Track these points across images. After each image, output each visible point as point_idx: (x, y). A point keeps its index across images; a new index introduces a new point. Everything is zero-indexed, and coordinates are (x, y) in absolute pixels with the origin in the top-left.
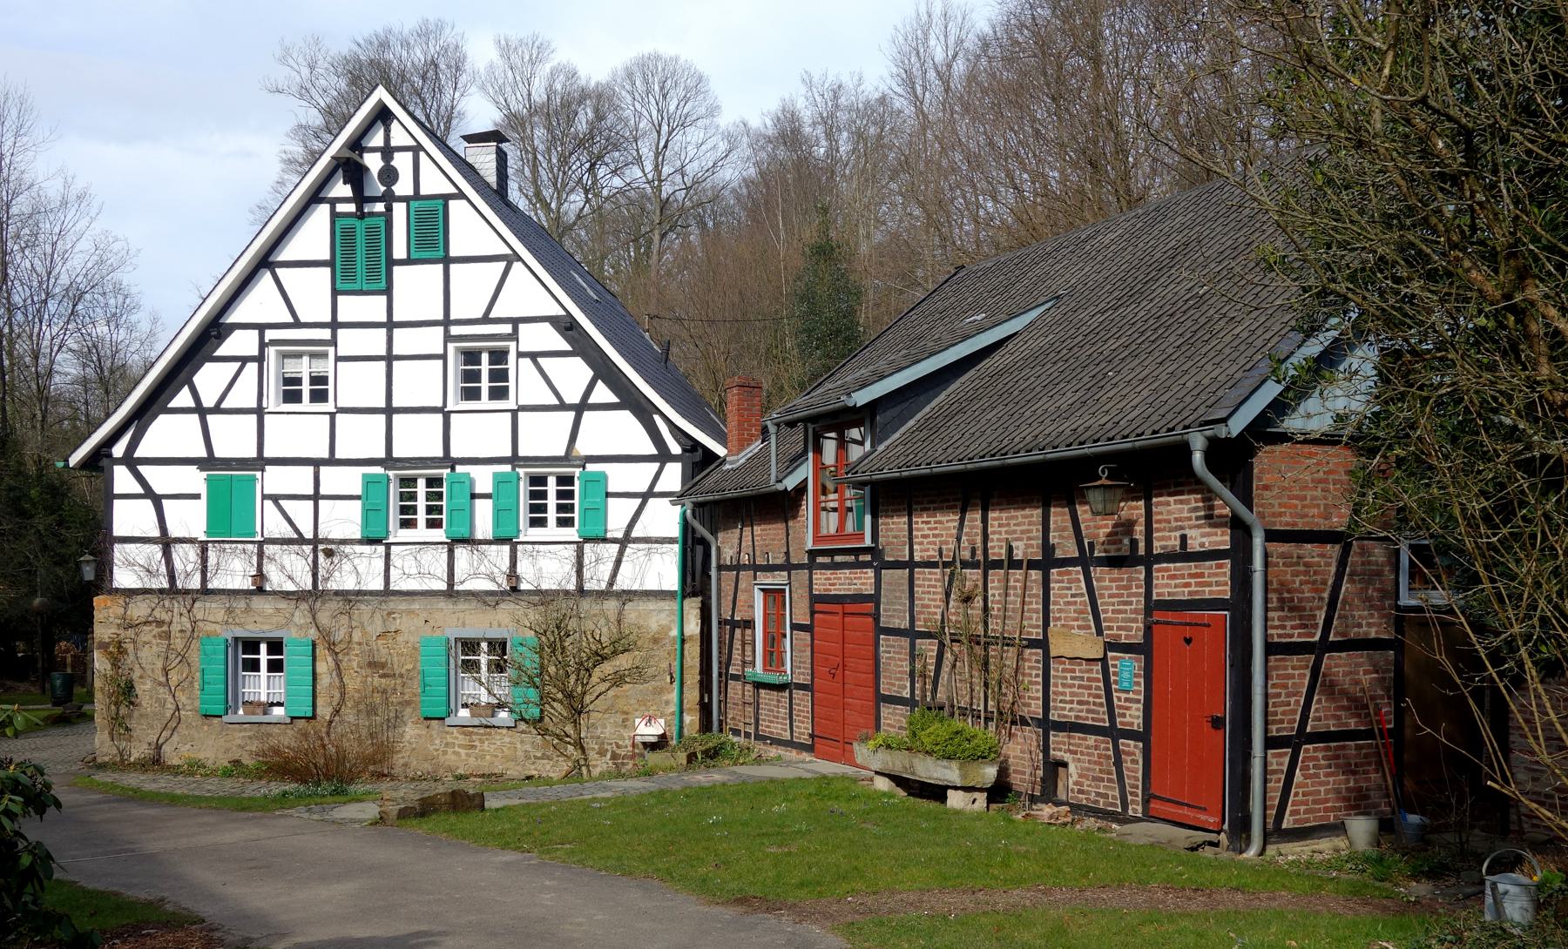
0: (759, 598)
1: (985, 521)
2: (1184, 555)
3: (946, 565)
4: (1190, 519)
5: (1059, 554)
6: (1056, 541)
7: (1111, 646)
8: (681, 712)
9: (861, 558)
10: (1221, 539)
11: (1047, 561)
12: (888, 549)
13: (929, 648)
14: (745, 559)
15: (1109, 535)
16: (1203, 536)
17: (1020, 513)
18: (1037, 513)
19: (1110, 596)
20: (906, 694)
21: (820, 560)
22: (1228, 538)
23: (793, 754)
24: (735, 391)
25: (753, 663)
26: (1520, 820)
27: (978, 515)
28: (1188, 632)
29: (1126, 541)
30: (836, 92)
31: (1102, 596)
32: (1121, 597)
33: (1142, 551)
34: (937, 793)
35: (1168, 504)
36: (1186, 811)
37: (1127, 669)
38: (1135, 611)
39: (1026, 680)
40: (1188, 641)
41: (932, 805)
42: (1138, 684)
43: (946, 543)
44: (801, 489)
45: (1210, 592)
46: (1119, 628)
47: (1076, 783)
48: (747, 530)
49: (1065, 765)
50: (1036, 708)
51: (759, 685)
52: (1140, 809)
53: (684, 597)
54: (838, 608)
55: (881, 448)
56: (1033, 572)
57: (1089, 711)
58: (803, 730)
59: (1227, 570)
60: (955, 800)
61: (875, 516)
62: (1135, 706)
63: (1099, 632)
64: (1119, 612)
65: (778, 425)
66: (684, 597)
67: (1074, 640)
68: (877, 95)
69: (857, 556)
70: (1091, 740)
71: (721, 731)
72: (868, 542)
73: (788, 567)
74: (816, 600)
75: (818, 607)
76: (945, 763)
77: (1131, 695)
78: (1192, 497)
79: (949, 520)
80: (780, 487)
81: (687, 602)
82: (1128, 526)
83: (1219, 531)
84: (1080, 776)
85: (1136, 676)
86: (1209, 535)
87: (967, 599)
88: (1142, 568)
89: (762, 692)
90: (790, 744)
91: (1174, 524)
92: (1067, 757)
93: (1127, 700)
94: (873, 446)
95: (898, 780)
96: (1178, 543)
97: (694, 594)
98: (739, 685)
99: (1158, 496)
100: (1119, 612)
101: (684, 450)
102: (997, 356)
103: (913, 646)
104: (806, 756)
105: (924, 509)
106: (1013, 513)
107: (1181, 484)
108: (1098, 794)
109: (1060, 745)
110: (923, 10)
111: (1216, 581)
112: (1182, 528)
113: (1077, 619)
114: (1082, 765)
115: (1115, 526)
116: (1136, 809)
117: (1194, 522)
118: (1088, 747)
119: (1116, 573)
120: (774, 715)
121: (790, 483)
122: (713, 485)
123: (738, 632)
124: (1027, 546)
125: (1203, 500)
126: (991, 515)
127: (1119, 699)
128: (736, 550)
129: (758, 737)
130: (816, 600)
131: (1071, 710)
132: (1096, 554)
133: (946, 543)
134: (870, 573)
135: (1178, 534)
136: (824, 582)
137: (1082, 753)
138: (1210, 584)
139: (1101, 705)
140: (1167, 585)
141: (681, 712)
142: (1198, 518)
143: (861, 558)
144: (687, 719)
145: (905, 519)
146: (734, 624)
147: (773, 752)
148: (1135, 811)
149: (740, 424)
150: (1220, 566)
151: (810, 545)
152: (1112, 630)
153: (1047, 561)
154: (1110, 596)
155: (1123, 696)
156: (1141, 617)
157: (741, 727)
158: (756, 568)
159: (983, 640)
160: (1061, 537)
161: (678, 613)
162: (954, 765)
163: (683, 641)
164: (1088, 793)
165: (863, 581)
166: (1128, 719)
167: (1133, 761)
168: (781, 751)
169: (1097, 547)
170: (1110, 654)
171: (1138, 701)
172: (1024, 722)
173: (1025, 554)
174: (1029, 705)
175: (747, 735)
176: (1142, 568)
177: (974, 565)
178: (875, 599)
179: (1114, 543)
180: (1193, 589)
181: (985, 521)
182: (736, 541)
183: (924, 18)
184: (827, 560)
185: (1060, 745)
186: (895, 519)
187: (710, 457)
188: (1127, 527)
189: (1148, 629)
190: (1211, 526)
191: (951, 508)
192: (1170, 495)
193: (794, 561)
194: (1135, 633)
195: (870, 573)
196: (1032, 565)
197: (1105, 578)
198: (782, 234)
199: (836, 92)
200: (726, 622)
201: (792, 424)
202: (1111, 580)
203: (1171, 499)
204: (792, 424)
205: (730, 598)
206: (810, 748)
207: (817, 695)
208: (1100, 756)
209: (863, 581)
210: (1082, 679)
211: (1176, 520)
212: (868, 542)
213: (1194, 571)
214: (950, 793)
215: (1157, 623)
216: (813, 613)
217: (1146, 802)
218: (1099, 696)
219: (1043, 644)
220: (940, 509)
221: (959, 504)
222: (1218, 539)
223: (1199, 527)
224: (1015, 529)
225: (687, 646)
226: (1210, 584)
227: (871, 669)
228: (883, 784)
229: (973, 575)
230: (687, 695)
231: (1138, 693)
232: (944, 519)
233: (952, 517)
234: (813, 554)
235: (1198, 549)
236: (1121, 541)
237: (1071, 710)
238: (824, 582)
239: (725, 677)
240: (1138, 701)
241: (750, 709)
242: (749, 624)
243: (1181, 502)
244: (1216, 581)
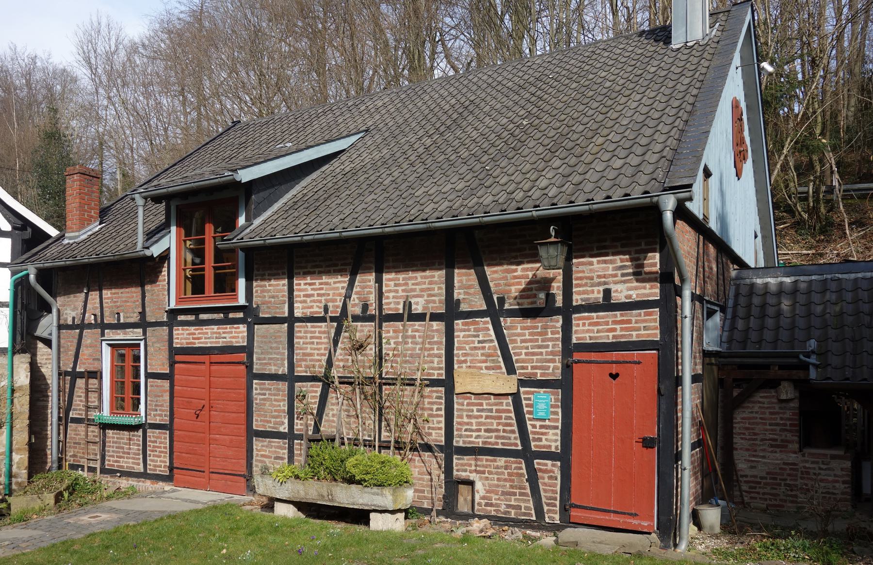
0: (107, 352)
1: (379, 281)
2: (607, 304)
3: (333, 319)
4: (615, 276)
5: (464, 307)
6: (461, 297)
7: (522, 383)
8: (11, 452)
9: (231, 315)
10: (652, 291)
11: (451, 313)
12: (263, 308)
13: (314, 391)
14: (90, 318)
15: (524, 290)
16: (629, 289)
17: (419, 275)
18: (439, 275)
19: (523, 341)
20: (284, 428)
21: (181, 318)
22: (658, 291)
23: (147, 485)
24: (75, 177)
25: (99, 408)
26: (742, 496)
27: (372, 277)
28: (614, 369)
29: (542, 296)
30: (34, 60)
31: (515, 341)
32: (537, 345)
33: (559, 302)
34: (361, 516)
35: (591, 264)
36: (612, 517)
37: (543, 405)
38: (552, 353)
39: (426, 414)
40: (614, 376)
41: (360, 529)
42: (556, 413)
43: (334, 301)
44: (165, 257)
45: (638, 336)
46: (533, 368)
47: (483, 498)
48: (94, 296)
49: (471, 483)
50: (437, 436)
51: (105, 427)
52: (557, 517)
53: (14, 353)
54: (205, 358)
55: (257, 222)
56: (434, 323)
57: (497, 437)
58: (159, 462)
59: (657, 317)
60: (377, 522)
61: (249, 280)
62: (551, 432)
63: (511, 370)
64: (533, 354)
65: (145, 198)
66: (14, 353)
67: (481, 376)
68: (61, 67)
69: (197, 315)
70: (501, 461)
71: (60, 467)
72: (242, 301)
73: (143, 324)
74: (174, 352)
75: (178, 358)
76: (375, 489)
77: (547, 423)
78: (617, 258)
79: (337, 284)
80: (148, 253)
81: (17, 357)
82: (545, 284)
83: (648, 285)
84: (488, 492)
85: (552, 406)
86: (636, 288)
87: (359, 347)
88: (560, 318)
89: (110, 433)
90: (144, 475)
91: (596, 280)
92: (473, 476)
93: (541, 427)
94: (248, 219)
95: (300, 506)
96: (601, 295)
97: (23, 351)
98: (81, 428)
99: (576, 258)
100: (533, 354)
101: (14, 228)
102: (335, 163)
103: (291, 389)
104: (167, 487)
105: (306, 274)
106: (411, 274)
107: (605, 247)
108: (508, 506)
109: (463, 467)
110: (95, 19)
111: (647, 326)
112: (605, 283)
113: (485, 361)
114: (491, 484)
115: (529, 283)
116: (553, 516)
117: (619, 278)
118: (497, 467)
119: (529, 322)
120: (123, 451)
121: (156, 250)
122: (50, 257)
123: (80, 383)
124: (428, 302)
125: (631, 260)
126: (385, 276)
127: (534, 426)
128: (80, 310)
129: (104, 471)
130: (175, 353)
131: (477, 437)
132: (507, 306)
133: (334, 301)
134: (243, 328)
135: (601, 288)
136: (183, 336)
137: (490, 473)
138: (639, 329)
139: (513, 432)
140: (588, 331)
141: (11, 452)
142: (623, 275)
143: (231, 315)
144: (16, 457)
145: (286, 282)
146: (75, 375)
147: (124, 483)
148: (553, 519)
149: (81, 206)
150: (650, 314)
151: (173, 305)
152: (526, 366)
153: (451, 313)
154: (523, 341)
155: (538, 424)
156: (558, 358)
157: (84, 462)
158: (103, 326)
159: (378, 381)
160: (466, 293)
161: (9, 367)
162: (387, 491)
163: (13, 391)
164: (498, 505)
165: (236, 335)
166: (544, 443)
167: (550, 478)
168: (132, 482)
169: (507, 301)
170: (522, 390)
171: (556, 428)
172: (428, 448)
173: (424, 308)
174: (430, 434)
175: (92, 470)
176: (560, 318)
177: (364, 318)
178: (248, 350)
179: (528, 297)
180: (618, 333)
181: (379, 281)
182: (81, 304)
183: (96, 24)
184: (190, 318)
185: (463, 467)
186: (273, 282)
187: (40, 236)
188: (545, 284)
189: (567, 368)
190: (638, 281)
191: (340, 272)
192: (592, 256)
193: (150, 318)
194: (554, 369)
195: (243, 328)
196: (435, 317)
197: (518, 330)
198: (16, 126)
199: (34, 60)
200: (67, 373)
201: (157, 199)
202: (523, 328)
203: (595, 260)
204: (157, 199)
205: (72, 353)
206: (169, 479)
207: (176, 433)
208: (509, 474)
209: (236, 335)
210: (491, 411)
211: (599, 277)
212: (242, 301)
213: (619, 318)
214: (372, 516)
215: (579, 362)
216: (172, 365)
217: (565, 510)
218: (510, 425)
219: (448, 383)
220: (328, 273)
221: (349, 268)
222: (647, 291)
223: (624, 282)
224: (417, 288)
225: (16, 395)
226: (639, 329)
227: (244, 408)
228: (284, 511)
229: (364, 329)
230: (16, 437)
231: (557, 420)
232: (331, 281)
233: (340, 278)
234: (173, 313)
235: (624, 300)
236: (535, 296)
237: (477, 437)
238: (183, 336)
239: (65, 420)
240: (556, 428)
241: (97, 448)
242: (96, 374)
243: (605, 262)
244: (647, 326)
